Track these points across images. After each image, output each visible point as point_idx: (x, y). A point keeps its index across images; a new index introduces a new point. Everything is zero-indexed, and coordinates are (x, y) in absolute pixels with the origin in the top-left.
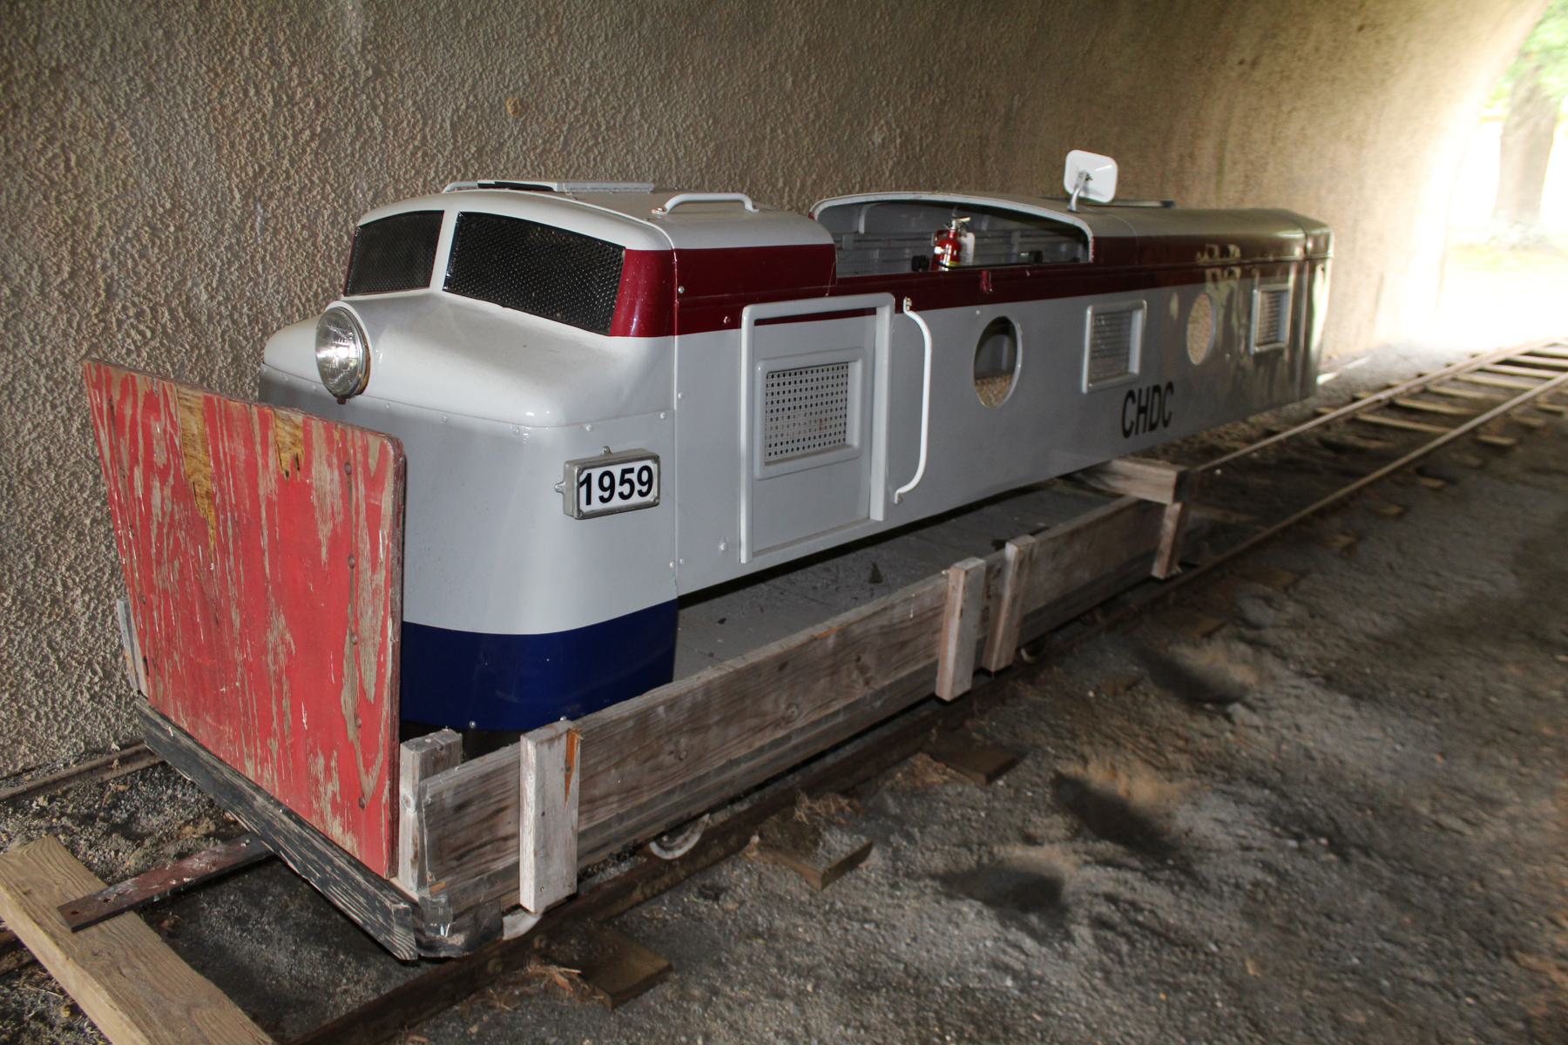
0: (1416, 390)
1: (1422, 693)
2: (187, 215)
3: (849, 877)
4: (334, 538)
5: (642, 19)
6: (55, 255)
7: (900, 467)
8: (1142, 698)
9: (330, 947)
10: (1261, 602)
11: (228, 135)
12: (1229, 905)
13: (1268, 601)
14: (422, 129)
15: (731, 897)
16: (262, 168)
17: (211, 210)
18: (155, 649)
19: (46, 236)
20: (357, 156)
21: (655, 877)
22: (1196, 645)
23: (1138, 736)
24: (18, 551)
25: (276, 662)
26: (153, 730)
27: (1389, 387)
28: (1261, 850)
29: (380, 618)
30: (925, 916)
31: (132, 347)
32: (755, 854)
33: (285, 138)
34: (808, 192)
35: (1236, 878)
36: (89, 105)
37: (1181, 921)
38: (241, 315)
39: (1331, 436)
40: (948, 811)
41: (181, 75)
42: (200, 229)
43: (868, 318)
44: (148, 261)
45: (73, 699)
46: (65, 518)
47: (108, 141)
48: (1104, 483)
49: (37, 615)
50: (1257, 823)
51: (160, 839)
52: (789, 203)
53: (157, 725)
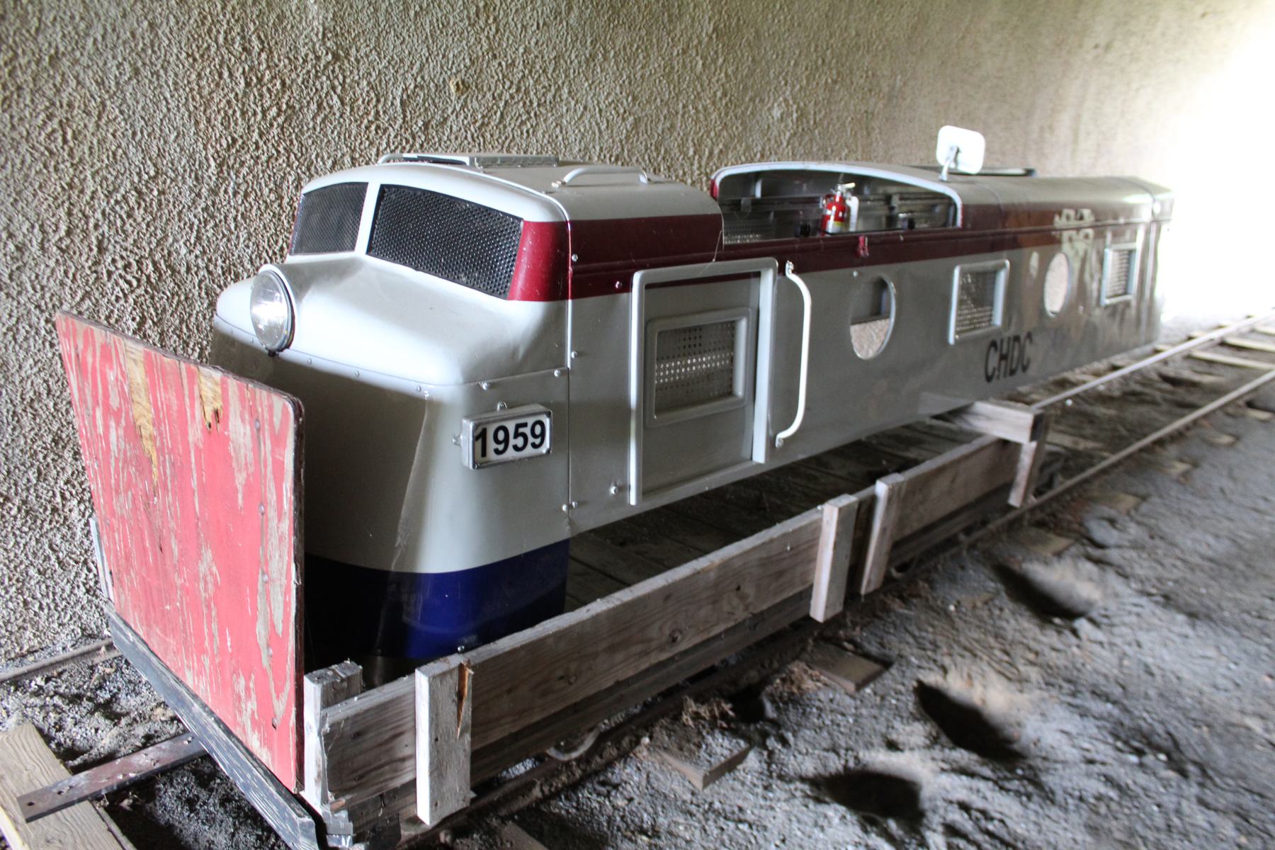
0: (1245, 330)
1: (1254, 613)
2: (168, 181)
3: (728, 778)
4: (248, 487)
5: (570, 9)
6: (54, 215)
7: (782, 411)
8: (997, 612)
9: (263, 831)
10: (1106, 524)
11: (205, 111)
12: (1074, 818)
13: (1112, 522)
14: (376, 106)
15: (621, 793)
16: (234, 140)
17: (190, 177)
18: (118, 566)
19: (46, 199)
20: (318, 129)
21: (553, 776)
22: (1046, 563)
23: (992, 648)
24: (22, 468)
25: (206, 590)
26: (118, 632)
27: (1220, 327)
28: (1103, 763)
29: (285, 562)
30: (793, 819)
31: (121, 295)
32: (645, 753)
33: (255, 114)
34: (715, 160)
35: (1080, 791)
36: (83, 87)
37: (1028, 831)
38: (216, 265)
39: (1170, 371)
40: (819, 716)
41: (165, 60)
42: (180, 193)
43: (753, 280)
44: (135, 220)
45: (72, 592)
46: (63, 440)
47: (100, 117)
48: (970, 424)
49: (39, 522)
50: (1100, 737)
51: (135, 720)
52: (699, 168)
53: (120, 630)
